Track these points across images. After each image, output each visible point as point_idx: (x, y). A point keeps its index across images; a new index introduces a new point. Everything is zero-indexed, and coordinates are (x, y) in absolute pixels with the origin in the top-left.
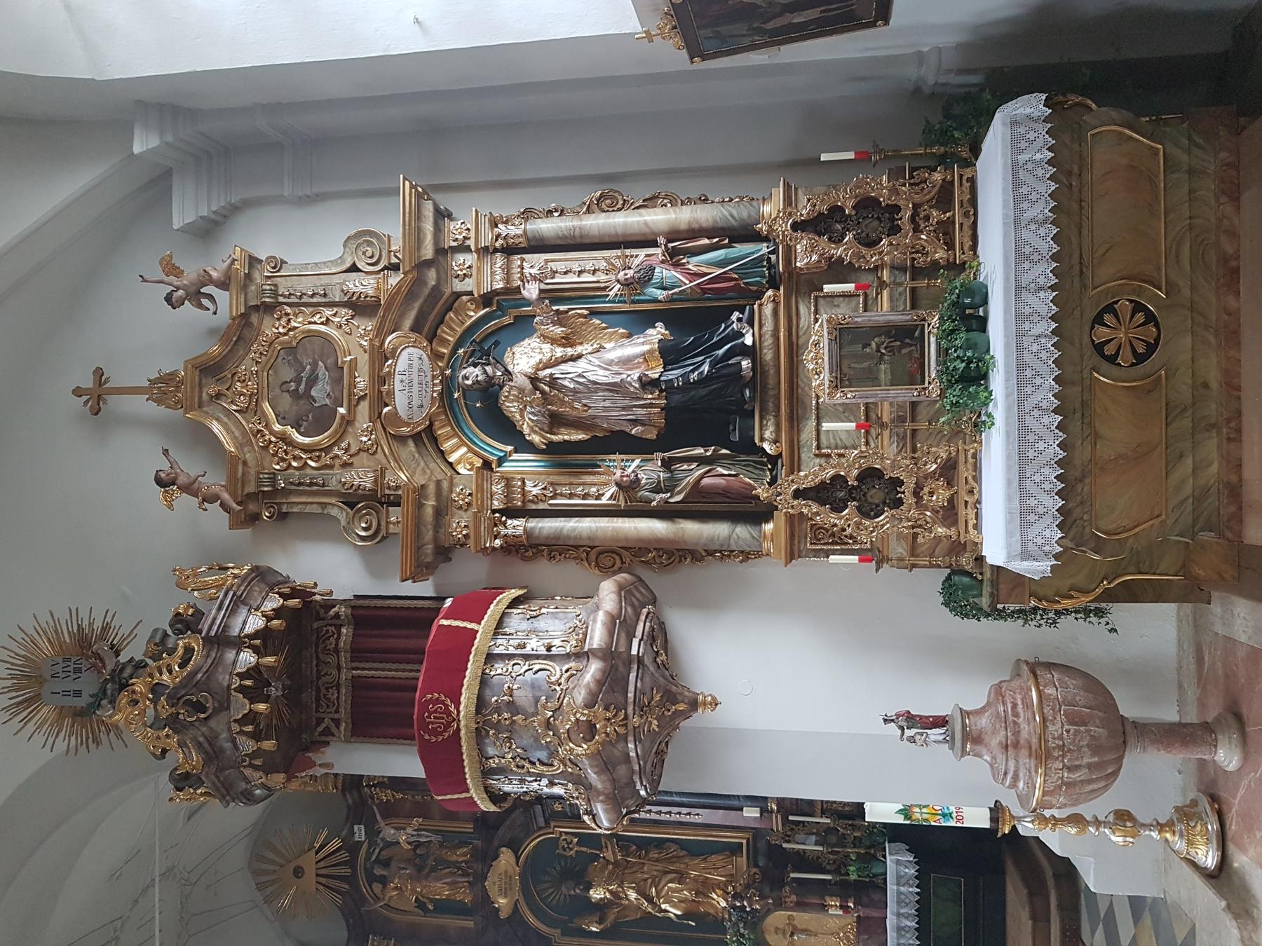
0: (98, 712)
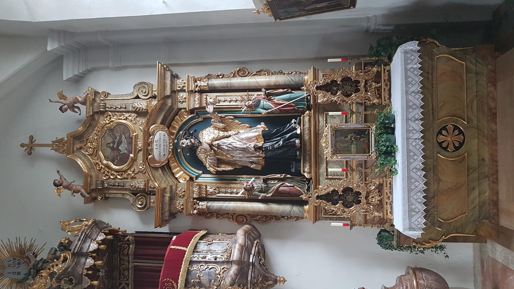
0: (27, 281)
